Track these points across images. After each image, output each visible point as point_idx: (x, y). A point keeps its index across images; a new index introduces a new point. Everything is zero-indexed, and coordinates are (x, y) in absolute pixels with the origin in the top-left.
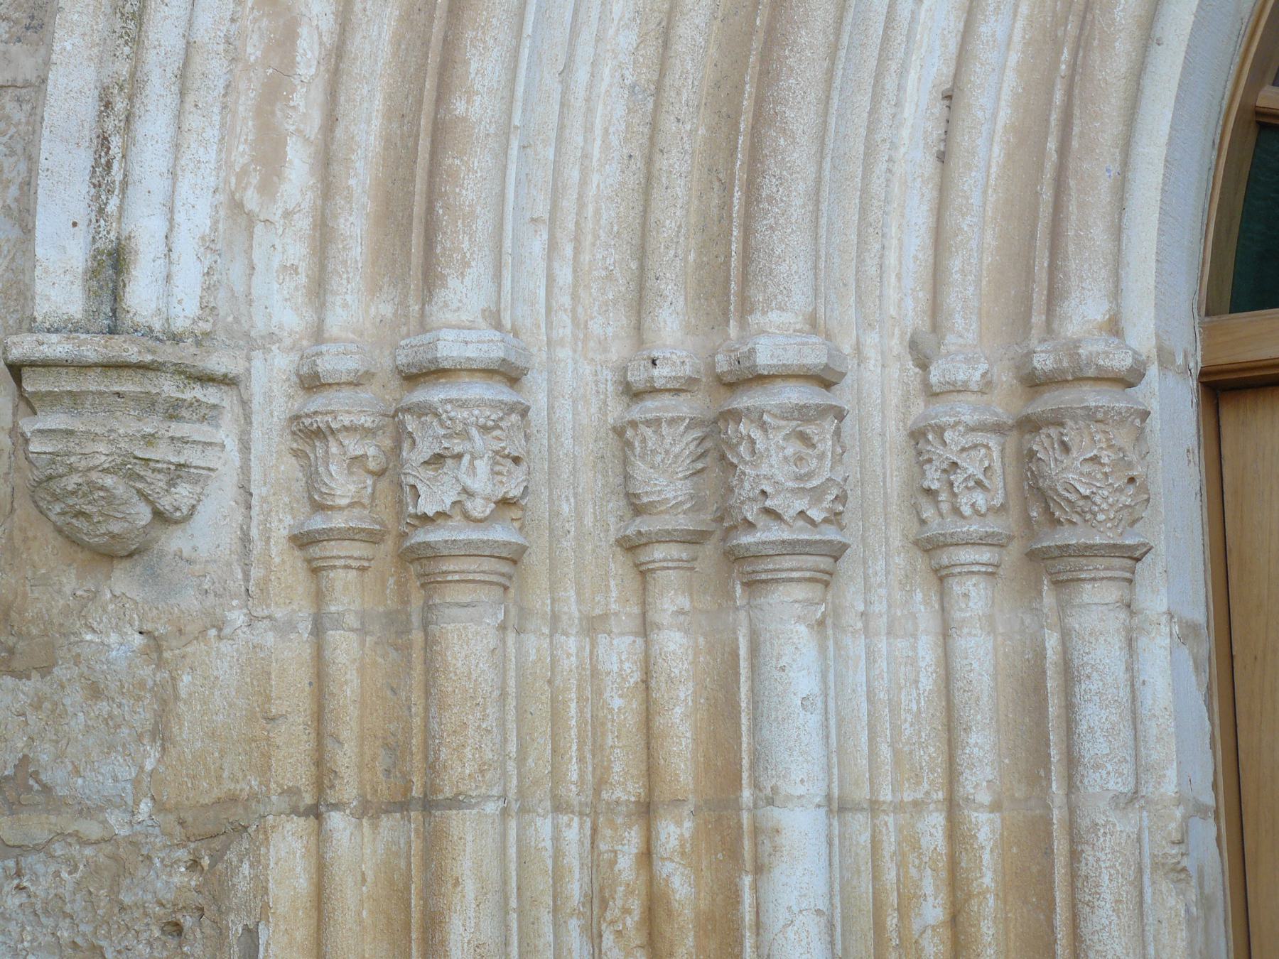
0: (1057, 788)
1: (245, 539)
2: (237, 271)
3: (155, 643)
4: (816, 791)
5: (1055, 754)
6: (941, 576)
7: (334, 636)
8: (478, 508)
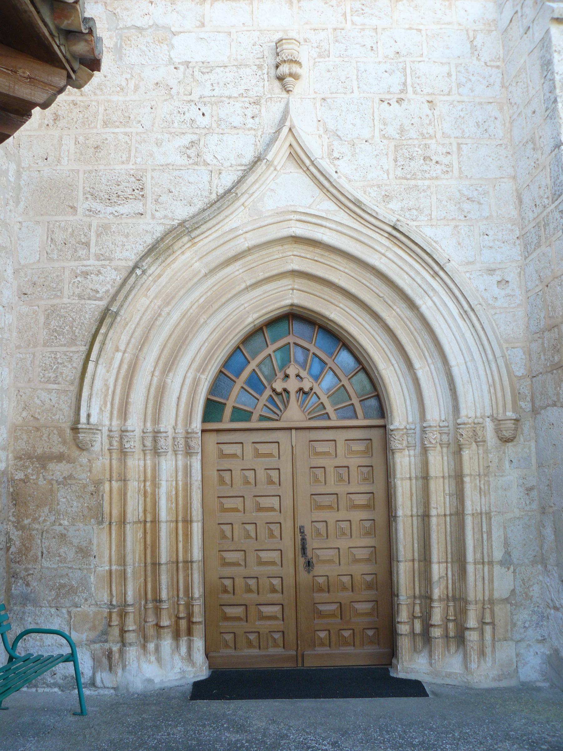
0: (189, 479)
1: (102, 449)
2: (101, 417)
3: (89, 461)
4: (165, 479)
5: (189, 475)
6: (176, 455)
7: (113, 461)
8: (132, 447)
